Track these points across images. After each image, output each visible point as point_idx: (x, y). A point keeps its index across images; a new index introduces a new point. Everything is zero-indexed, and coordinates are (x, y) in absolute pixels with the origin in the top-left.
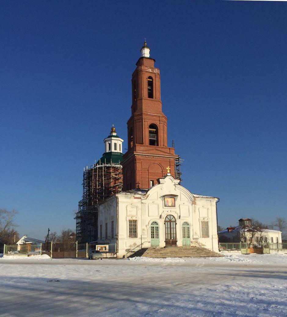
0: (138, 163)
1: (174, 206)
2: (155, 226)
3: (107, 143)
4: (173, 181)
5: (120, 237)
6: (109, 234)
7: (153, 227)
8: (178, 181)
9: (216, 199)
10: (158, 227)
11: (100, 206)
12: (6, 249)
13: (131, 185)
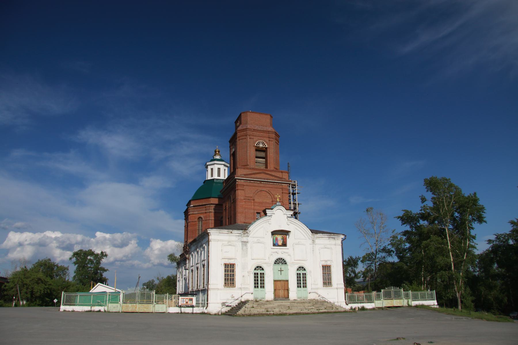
1: (284, 244)
2: (259, 272)
7: (257, 274)
9: (343, 237)
12: (63, 300)
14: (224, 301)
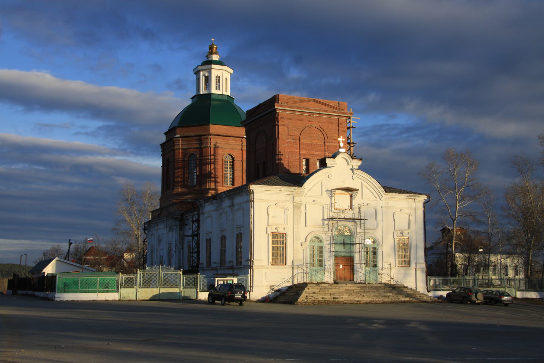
0: (281, 125)
3: (202, 73)
4: (350, 163)
5: (255, 264)
6: (231, 256)
8: (359, 163)
10: (283, 248)
11: (207, 204)
13: (267, 165)
14: (272, 284)
